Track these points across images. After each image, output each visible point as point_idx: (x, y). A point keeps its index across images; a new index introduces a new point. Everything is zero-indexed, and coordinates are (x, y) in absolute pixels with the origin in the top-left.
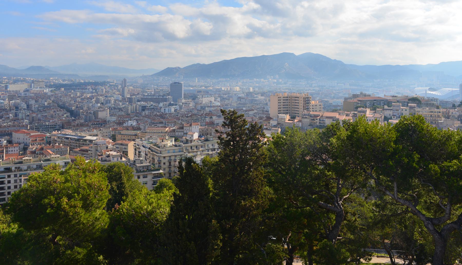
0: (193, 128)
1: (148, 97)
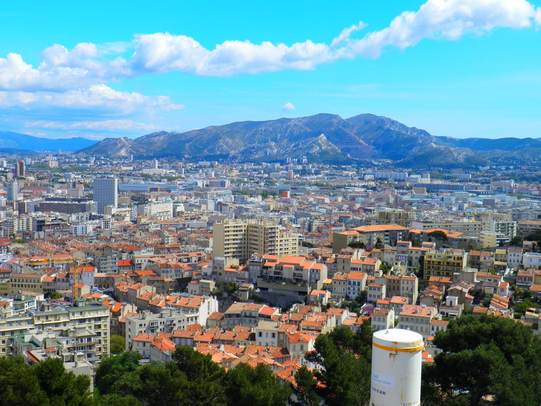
0: (85, 275)
1: (53, 202)
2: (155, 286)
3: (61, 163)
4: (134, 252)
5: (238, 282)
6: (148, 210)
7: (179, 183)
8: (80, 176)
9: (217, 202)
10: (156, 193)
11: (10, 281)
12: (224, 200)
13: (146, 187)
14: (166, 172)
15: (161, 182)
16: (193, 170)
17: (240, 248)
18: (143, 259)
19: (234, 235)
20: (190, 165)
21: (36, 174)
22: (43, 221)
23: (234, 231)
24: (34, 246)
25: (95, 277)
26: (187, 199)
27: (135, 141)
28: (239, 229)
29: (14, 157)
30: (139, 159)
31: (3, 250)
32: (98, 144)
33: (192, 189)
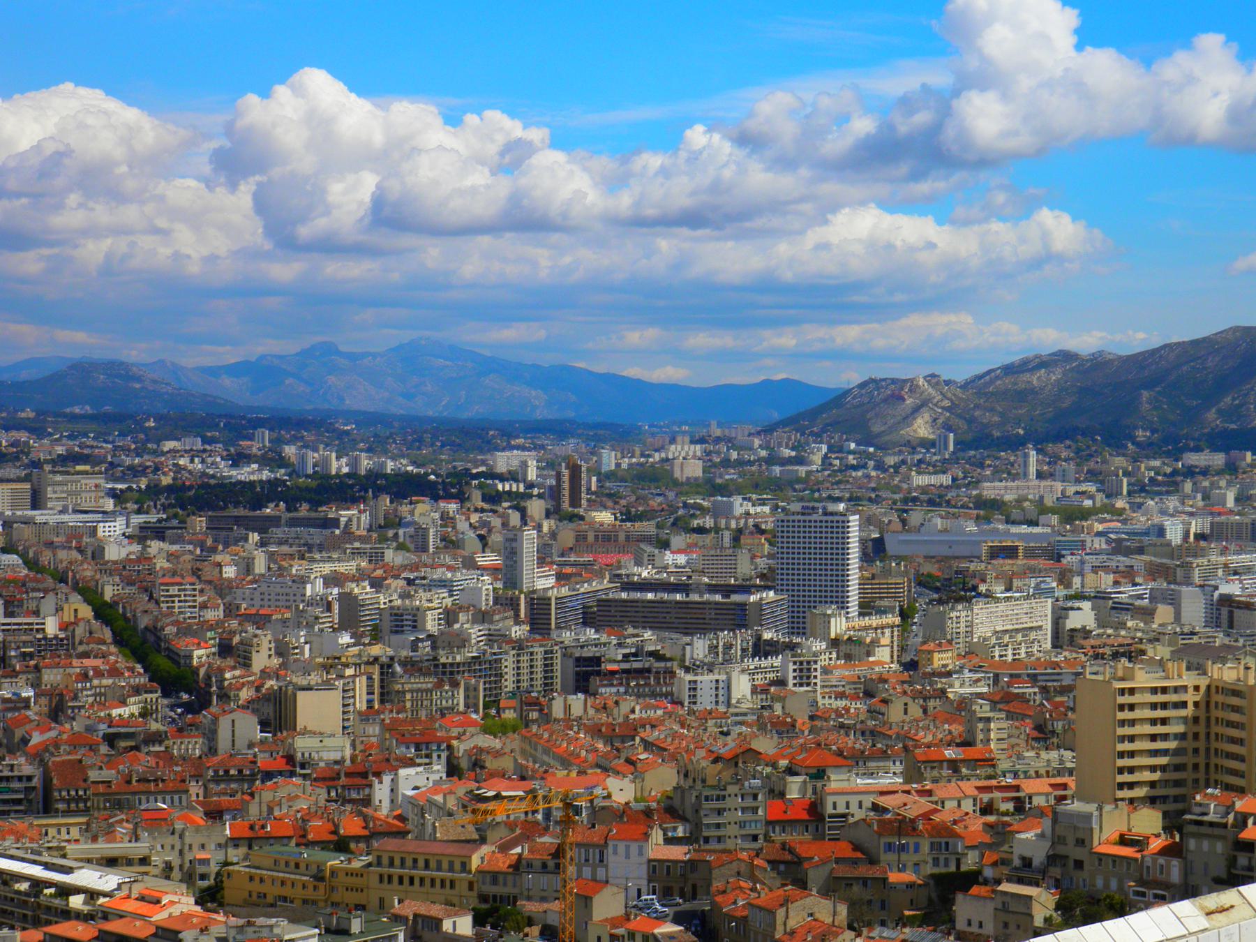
0: (615, 853)
1: (638, 595)
2: (844, 899)
3: (715, 465)
4: (829, 772)
5: (1143, 895)
6: (962, 625)
7: (1099, 527)
8: (767, 509)
9: (1216, 594)
10: (1007, 565)
11: (375, 862)
12: (1243, 589)
13: (978, 543)
14: (1063, 492)
15: (1037, 525)
16: (1159, 484)
17: (1178, 768)
18: (854, 801)
19: (1153, 722)
20: (1150, 467)
21: (623, 502)
22: (597, 661)
23: (1154, 706)
24: (536, 744)
25: (650, 861)
26: (1116, 583)
27: (965, 386)
28: (1174, 698)
29: (569, 447)
30: (976, 449)
31: (435, 755)
32: (839, 398)
33: (1141, 551)
